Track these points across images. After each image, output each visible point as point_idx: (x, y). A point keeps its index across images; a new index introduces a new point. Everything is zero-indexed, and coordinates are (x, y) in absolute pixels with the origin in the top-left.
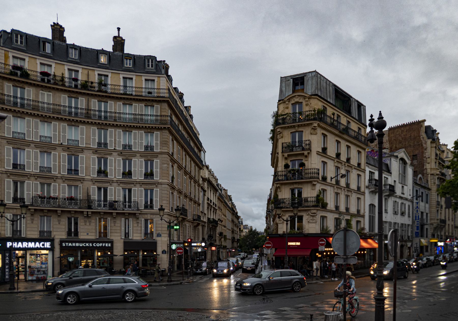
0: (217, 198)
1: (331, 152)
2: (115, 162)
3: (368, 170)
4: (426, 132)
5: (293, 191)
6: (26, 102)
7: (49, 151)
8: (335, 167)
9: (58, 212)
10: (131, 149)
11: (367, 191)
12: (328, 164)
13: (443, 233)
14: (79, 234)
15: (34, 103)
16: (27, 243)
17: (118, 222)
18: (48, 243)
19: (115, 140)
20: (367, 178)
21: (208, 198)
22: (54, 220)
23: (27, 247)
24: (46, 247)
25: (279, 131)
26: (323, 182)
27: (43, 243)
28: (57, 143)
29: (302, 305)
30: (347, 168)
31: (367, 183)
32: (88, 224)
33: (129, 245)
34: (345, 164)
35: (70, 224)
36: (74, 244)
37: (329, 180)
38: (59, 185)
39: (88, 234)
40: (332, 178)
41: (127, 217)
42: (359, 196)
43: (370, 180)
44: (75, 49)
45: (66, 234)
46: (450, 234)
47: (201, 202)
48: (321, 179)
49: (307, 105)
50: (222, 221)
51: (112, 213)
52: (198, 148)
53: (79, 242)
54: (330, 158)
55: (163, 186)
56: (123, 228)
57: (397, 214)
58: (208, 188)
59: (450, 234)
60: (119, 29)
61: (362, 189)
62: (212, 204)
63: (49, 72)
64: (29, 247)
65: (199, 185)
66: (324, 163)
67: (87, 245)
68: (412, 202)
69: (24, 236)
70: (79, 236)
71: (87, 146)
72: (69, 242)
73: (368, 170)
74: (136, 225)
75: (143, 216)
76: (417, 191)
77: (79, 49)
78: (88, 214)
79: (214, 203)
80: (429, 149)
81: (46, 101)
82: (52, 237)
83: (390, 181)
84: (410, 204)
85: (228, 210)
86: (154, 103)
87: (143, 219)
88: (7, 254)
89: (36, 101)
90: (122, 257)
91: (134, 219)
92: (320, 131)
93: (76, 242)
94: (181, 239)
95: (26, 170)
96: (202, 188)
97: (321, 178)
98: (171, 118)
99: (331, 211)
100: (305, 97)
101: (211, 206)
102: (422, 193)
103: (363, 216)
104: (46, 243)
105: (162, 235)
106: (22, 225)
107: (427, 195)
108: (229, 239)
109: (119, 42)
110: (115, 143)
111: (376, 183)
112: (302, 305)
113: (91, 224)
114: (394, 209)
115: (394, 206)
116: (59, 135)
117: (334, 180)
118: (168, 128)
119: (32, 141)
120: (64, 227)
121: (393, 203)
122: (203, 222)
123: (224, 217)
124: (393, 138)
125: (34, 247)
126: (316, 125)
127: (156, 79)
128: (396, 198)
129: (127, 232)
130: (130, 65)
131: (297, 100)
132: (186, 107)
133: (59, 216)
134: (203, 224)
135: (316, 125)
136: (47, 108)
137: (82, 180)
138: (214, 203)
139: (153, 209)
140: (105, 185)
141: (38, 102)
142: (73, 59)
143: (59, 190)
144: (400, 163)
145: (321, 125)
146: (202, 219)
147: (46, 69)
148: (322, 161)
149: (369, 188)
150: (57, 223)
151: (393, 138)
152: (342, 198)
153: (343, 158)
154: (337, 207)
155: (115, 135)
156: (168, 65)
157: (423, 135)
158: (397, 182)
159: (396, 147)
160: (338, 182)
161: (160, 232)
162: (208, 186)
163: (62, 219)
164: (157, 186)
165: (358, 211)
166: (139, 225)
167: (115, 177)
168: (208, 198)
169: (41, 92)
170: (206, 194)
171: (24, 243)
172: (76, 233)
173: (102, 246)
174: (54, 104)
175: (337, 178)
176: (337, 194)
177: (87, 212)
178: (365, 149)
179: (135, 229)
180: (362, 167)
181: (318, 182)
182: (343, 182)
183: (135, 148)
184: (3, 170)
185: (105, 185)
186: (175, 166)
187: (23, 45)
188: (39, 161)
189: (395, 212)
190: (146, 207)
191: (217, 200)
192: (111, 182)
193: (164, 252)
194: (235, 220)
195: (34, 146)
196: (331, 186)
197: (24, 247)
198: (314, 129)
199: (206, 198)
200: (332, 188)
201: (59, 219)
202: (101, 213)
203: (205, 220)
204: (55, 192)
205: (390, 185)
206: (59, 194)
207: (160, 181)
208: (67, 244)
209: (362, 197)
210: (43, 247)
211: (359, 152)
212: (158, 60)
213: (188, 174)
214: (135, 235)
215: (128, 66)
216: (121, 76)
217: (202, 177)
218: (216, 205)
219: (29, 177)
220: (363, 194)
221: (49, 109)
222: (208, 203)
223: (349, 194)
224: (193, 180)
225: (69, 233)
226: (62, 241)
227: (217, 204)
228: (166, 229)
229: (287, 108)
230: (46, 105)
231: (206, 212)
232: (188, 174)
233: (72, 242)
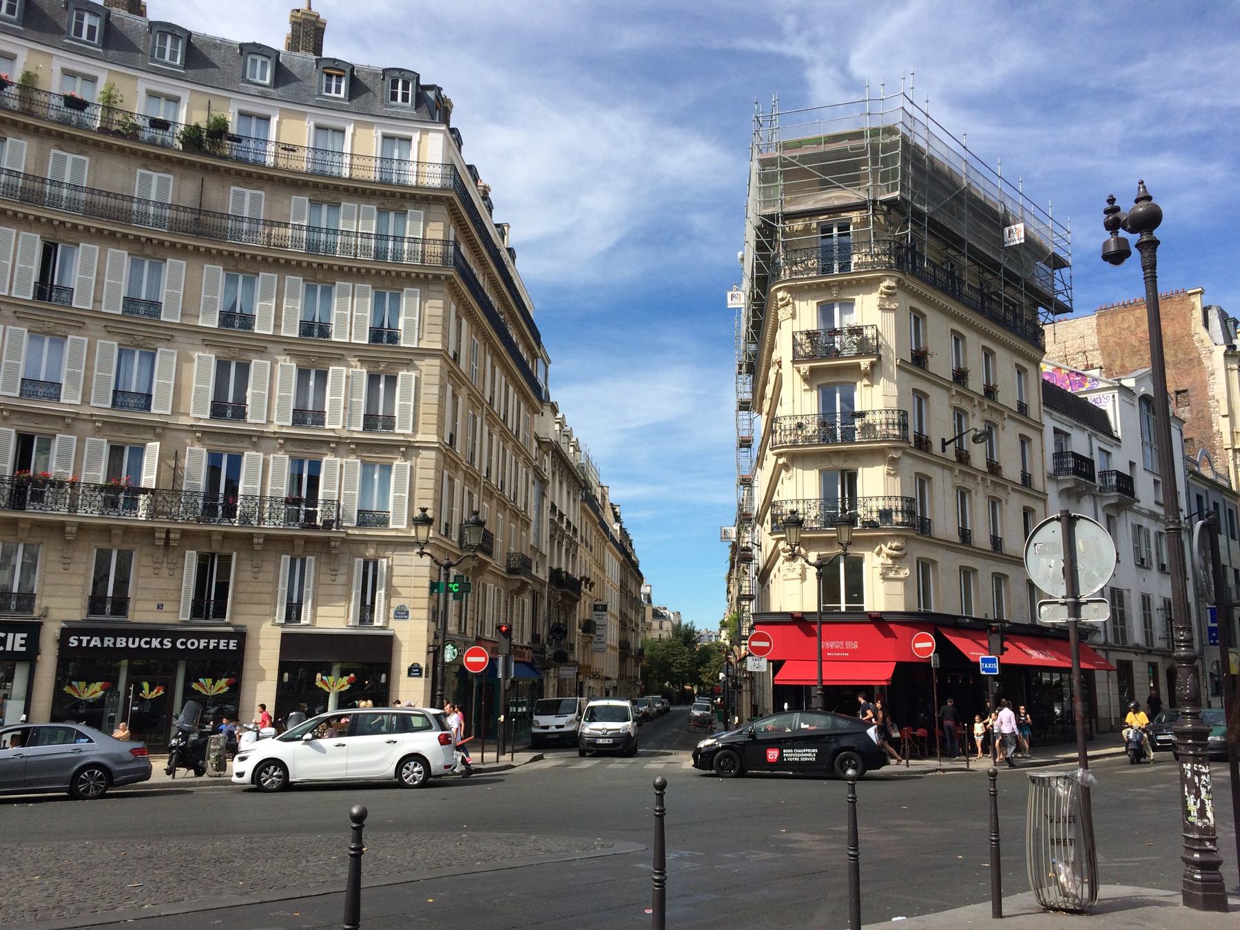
0: (578, 507)
1: (942, 363)
7: (61, 330)
8: (952, 411)
9: (68, 529)
10: (328, 335)
11: (1052, 491)
12: (931, 399)
14: (131, 606)
15: (29, 184)
17: (269, 567)
18: (19, 636)
20: (1050, 448)
21: (553, 507)
25: (782, 299)
26: (919, 454)
29: (900, 822)
30: (987, 416)
31: (1050, 467)
32: (165, 572)
34: (980, 404)
36: (109, 642)
37: (937, 448)
38: (81, 441)
39: (160, 607)
40: (944, 443)
42: (1030, 503)
43: (1060, 455)
44: (176, 38)
45: (87, 604)
47: (532, 514)
48: (913, 445)
50: (592, 585)
52: (529, 348)
54: (936, 381)
56: (283, 589)
57: (1148, 568)
58: (554, 474)
61: (1038, 482)
62: (564, 526)
63: (87, 98)
65: (528, 461)
66: (920, 396)
67: (155, 643)
70: (130, 613)
72: (91, 633)
76: (1199, 498)
77: (185, 36)
78: (167, 539)
79: (569, 523)
81: (246, 214)
82: (36, 614)
83: (1119, 463)
85: (610, 549)
86: (407, 204)
87: (359, 562)
89: (35, 178)
91: (324, 559)
93: (115, 633)
94: (469, 631)
96: (538, 472)
97: (912, 439)
98: (457, 249)
99: (948, 546)
101: (563, 532)
102: (1216, 505)
104: (10, 636)
107: (1231, 511)
108: (612, 648)
109: (308, 31)
111: (1067, 471)
112: (900, 822)
114: (1137, 550)
115: (1136, 540)
117: (951, 448)
118: (448, 277)
120: (80, 581)
121: (1134, 532)
122: (536, 579)
123: (599, 572)
124: (1112, 339)
127: (416, 137)
128: (1140, 517)
129: (295, 601)
132: (497, 226)
134: (537, 588)
138: (569, 523)
140: (234, 447)
141: (43, 180)
142: (166, 64)
144: (1141, 411)
145: (907, 283)
146: (534, 572)
147: (78, 90)
148: (915, 390)
149: (1058, 482)
150: (60, 568)
151: (1112, 339)
153: (976, 383)
154: (965, 535)
156: (448, 101)
158: (1139, 466)
159: (1123, 366)
160: (963, 457)
162: (554, 465)
163: (76, 554)
168: (553, 507)
169: (53, 151)
170: (549, 493)
171: (106, 639)
172: (121, 605)
173: (206, 647)
174: (92, 191)
175: (961, 443)
176: (963, 493)
177: (168, 532)
181: (905, 453)
183: (341, 333)
186: (463, 393)
187: (15, 17)
188: (22, 363)
189: (1142, 560)
191: (578, 513)
193: (414, 671)
194: (632, 585)
195: (11, 314)
196: (944, 467)
199: (547, 504)
200: (947, 472)
203: (543, 575)
205: (1119, 474)
208: (85, 639)
209: (1038, 506)
212: (422, 82)
213: (497, 423)
215: (333, 94)
217: (537, 439)
218: (575, 530)
221: (73, 205)
222: (552, 521)
223: (1000, 494)
224: (510, 444)
225: (96, 603)
226: (66, 633)
227: (578, 526)
228: (426, 592)
230: (65, 192)
231: (545, 549)
232: (497, 423)
233: (102, 633)
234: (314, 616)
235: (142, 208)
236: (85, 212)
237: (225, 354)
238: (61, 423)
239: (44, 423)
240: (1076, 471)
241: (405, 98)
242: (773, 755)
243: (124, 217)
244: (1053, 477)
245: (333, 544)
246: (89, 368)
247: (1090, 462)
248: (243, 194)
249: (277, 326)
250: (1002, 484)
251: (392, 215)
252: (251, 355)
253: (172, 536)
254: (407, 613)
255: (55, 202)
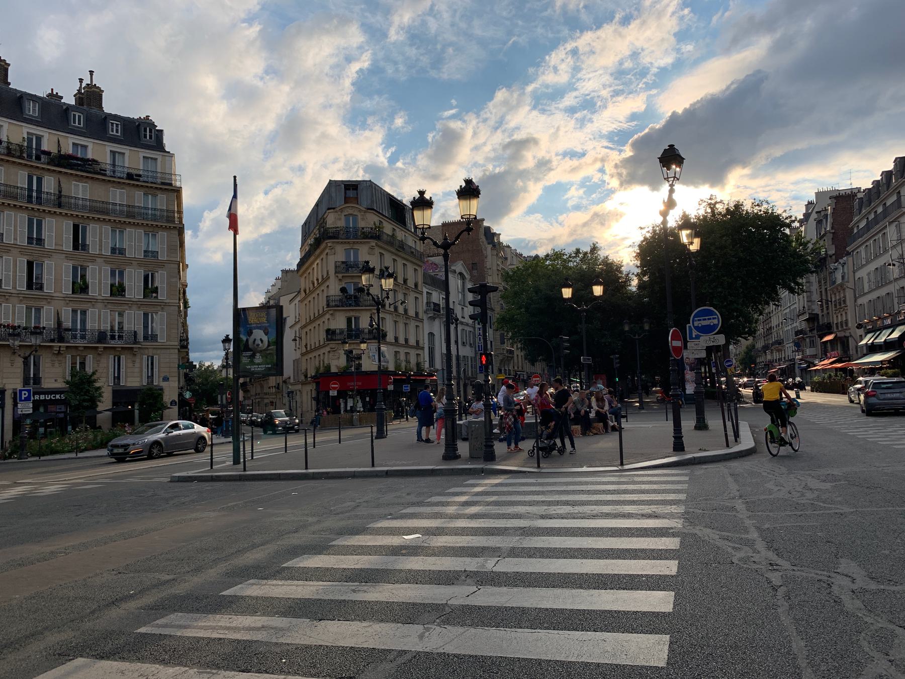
3: (425, 290)
4: (485, 234)
5: (349, 320)
11: (425, 318)
13: (511, 368)
19: (101, 241)
20: (425, 301)
32: (57, 365)
38: (14, 307)
41: (118, 353)
43: (428, 303)
46: (520, 369)
49: (363, 219)
51: (97, 347)
53: (45, 393)
59: (520, 369)
60: (91, 72)
67: (58, 397)
68: (474, 328)
71: (58, 248)
73: (425, 290)
74: (131, 365)
75: (146, 351)
80: (489, 257)
84: (472, 329)
90: (109, 413)
92: (377, 251)
100: (360, 211)
103: (423, 348)
110: (101, 246)
116: (15, 230)
126: (374, 244)
130: (117, 132)
131: (350, 211)
135: (374, 244)
137: (49, 299)
143: (14, 313)
152: (401, 326)
155: (101, 234)
157: (483, 238)
160: (396, 308)
161: (167, 374)
165: (417, 342)
166: (137, 365)
167: (100, 295)
178: (421, 266)
180: (420, 288)
182: (401, 309)
192: (93, 301)
198: (372, 248)
204: (7, 317)
206: (13, 320)
207: (167, 301)
211: (415, 270)
214: (129, 379)
215: (115, 133)
216: (108, 149)
220: (422, 321)
225: (26, 381)
228: (176, 370)
229: (340, 219)
234: (126, 381)
235: (146, 211)
237: (114, 267)
240: (434, 310)
241: (151, 137)
244: (426, 312)
246: (15, 272)
247: (439, 305)
249: (100, 250)
250: (398, 315)
251: (150, 196)
252: (89, 264)
255: (114, 211)
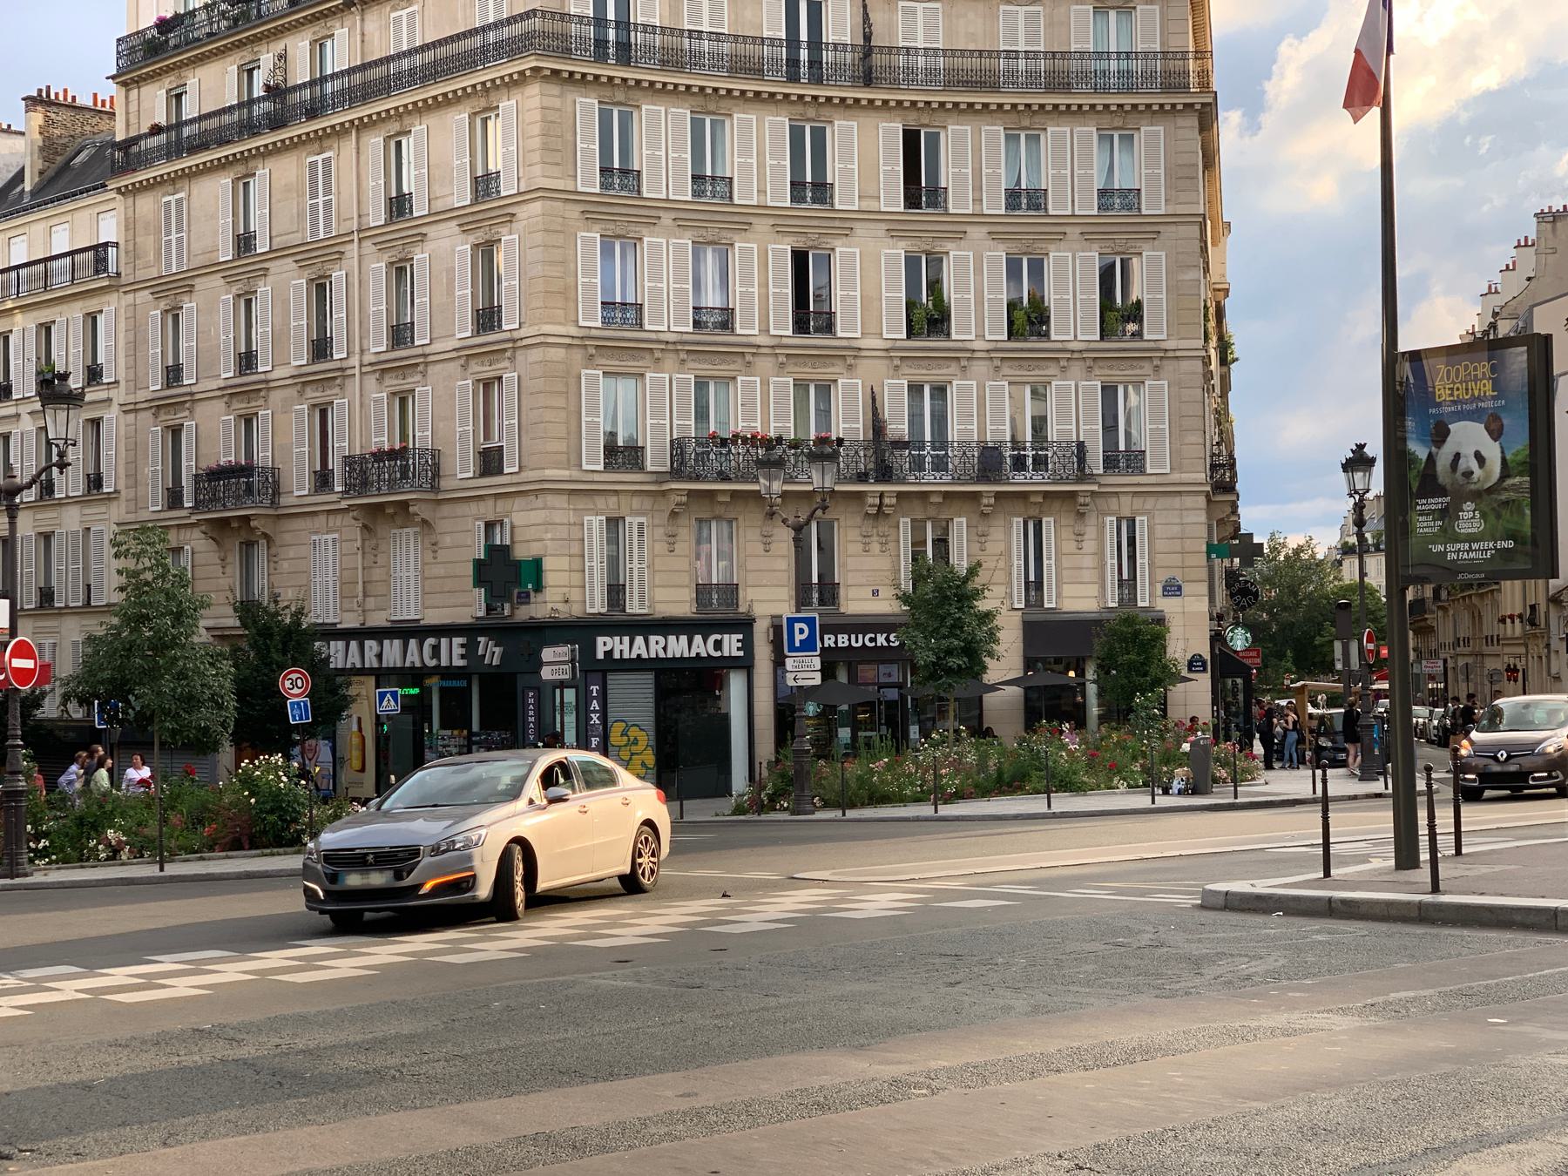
2: (979, 270)
6: (921, 61)
16: (661, 639)
17: (997, 533)
18: (735, 637)
19: (977, 173)
22: (749, 532)
23: (662, 655)
24: (726, 654)
27: (718, 637)
28: (856, 208)
32: (875, 547)
33: (1050, 639)
35: (801, 545)
38: (765, 383)
39: (875, 593)
55: (1185, 365)
56: (1018, 563)
64: (670, 655)
67: (881, 640)
69: (1146, 604)
71: (866, 205)
81: (706, 28)
82: (742, 609)
87: (1111, 520)
88: (595, 688)
95: (647, 327)
104: (726, 637)
105: (1186, 588)
106: (54, 567)
110: (978, 188)
113: (773, 547)
116: (761, 165)
119: (667, 200)
125: (686, 655)
133: (984, 515)
136: (712, 55)
139: (1142, 472)
140: (937, 374)
164: (1157, 368)
167: (765, 331)
171: (653, 639)
177: (882, 495)
179: (1066, 562)
184: (573, 331)
185: (937, 374)
190: (1111, 462)
192: (963, 358)
195: (767, 228)
197: (653, 655)
201: (767, 529)
202: (721, 499)
210: (718, 654)
214: (1067, 590)
219: (658, 354)
236: (663, 62)
238: (739, 360)
239: (724, 362)
242: (595, 688)
243: (987, 82)
245: (1081, 500)
248: (914, 12)
249: (978, 200)
253: (887, 501)
254: (1179, 588)
